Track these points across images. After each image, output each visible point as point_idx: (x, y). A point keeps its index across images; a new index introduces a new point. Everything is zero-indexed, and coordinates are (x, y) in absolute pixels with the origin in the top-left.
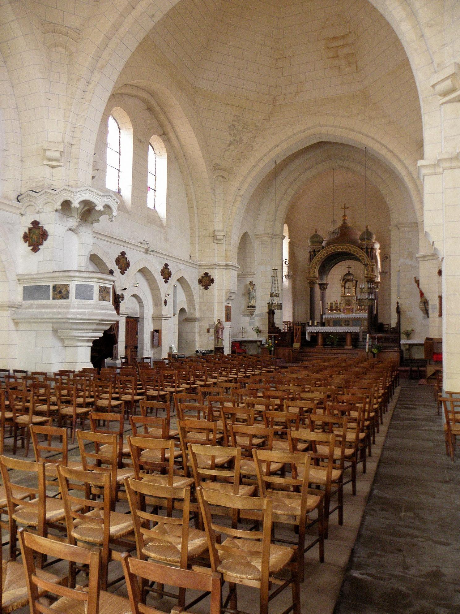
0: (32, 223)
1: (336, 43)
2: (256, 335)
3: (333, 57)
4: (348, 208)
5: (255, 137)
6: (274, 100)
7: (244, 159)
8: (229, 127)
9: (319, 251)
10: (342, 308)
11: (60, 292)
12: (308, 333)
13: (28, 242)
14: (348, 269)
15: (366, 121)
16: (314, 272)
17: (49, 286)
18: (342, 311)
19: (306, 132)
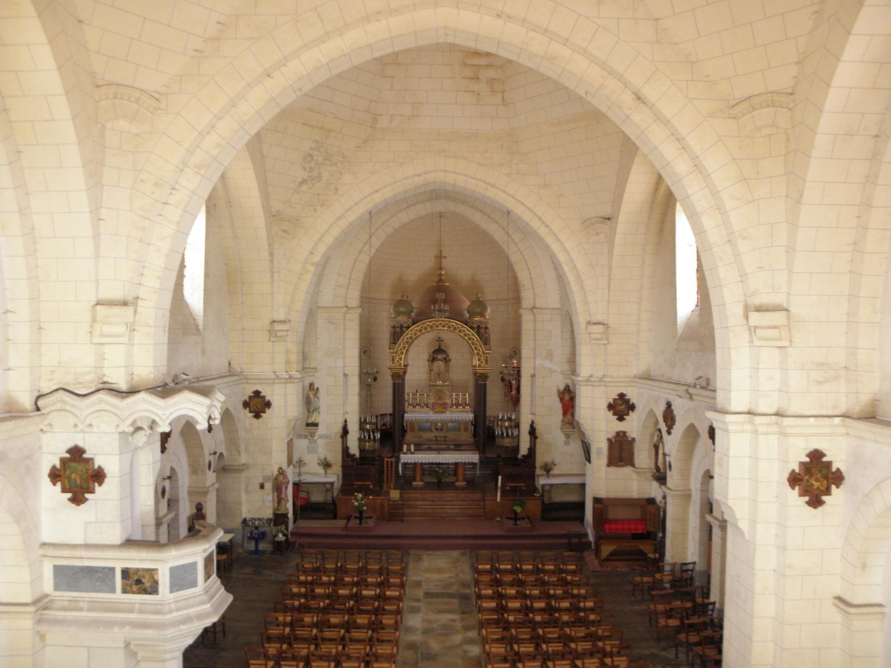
1: (477, 61)
2: (321, 470)
3: (472, 78)
5: (341, 173)
6: (375, 120)
7: (323, 205)
8: (304, 158)
9: (408, 327)
10: (431, 401)
11: (139, 582)
12: (402, 464)
13: (59, 484)
14: (438, 342)
16: (401, 359)
17: (112, 570)
18: (430, 406)
19: (422, 177)
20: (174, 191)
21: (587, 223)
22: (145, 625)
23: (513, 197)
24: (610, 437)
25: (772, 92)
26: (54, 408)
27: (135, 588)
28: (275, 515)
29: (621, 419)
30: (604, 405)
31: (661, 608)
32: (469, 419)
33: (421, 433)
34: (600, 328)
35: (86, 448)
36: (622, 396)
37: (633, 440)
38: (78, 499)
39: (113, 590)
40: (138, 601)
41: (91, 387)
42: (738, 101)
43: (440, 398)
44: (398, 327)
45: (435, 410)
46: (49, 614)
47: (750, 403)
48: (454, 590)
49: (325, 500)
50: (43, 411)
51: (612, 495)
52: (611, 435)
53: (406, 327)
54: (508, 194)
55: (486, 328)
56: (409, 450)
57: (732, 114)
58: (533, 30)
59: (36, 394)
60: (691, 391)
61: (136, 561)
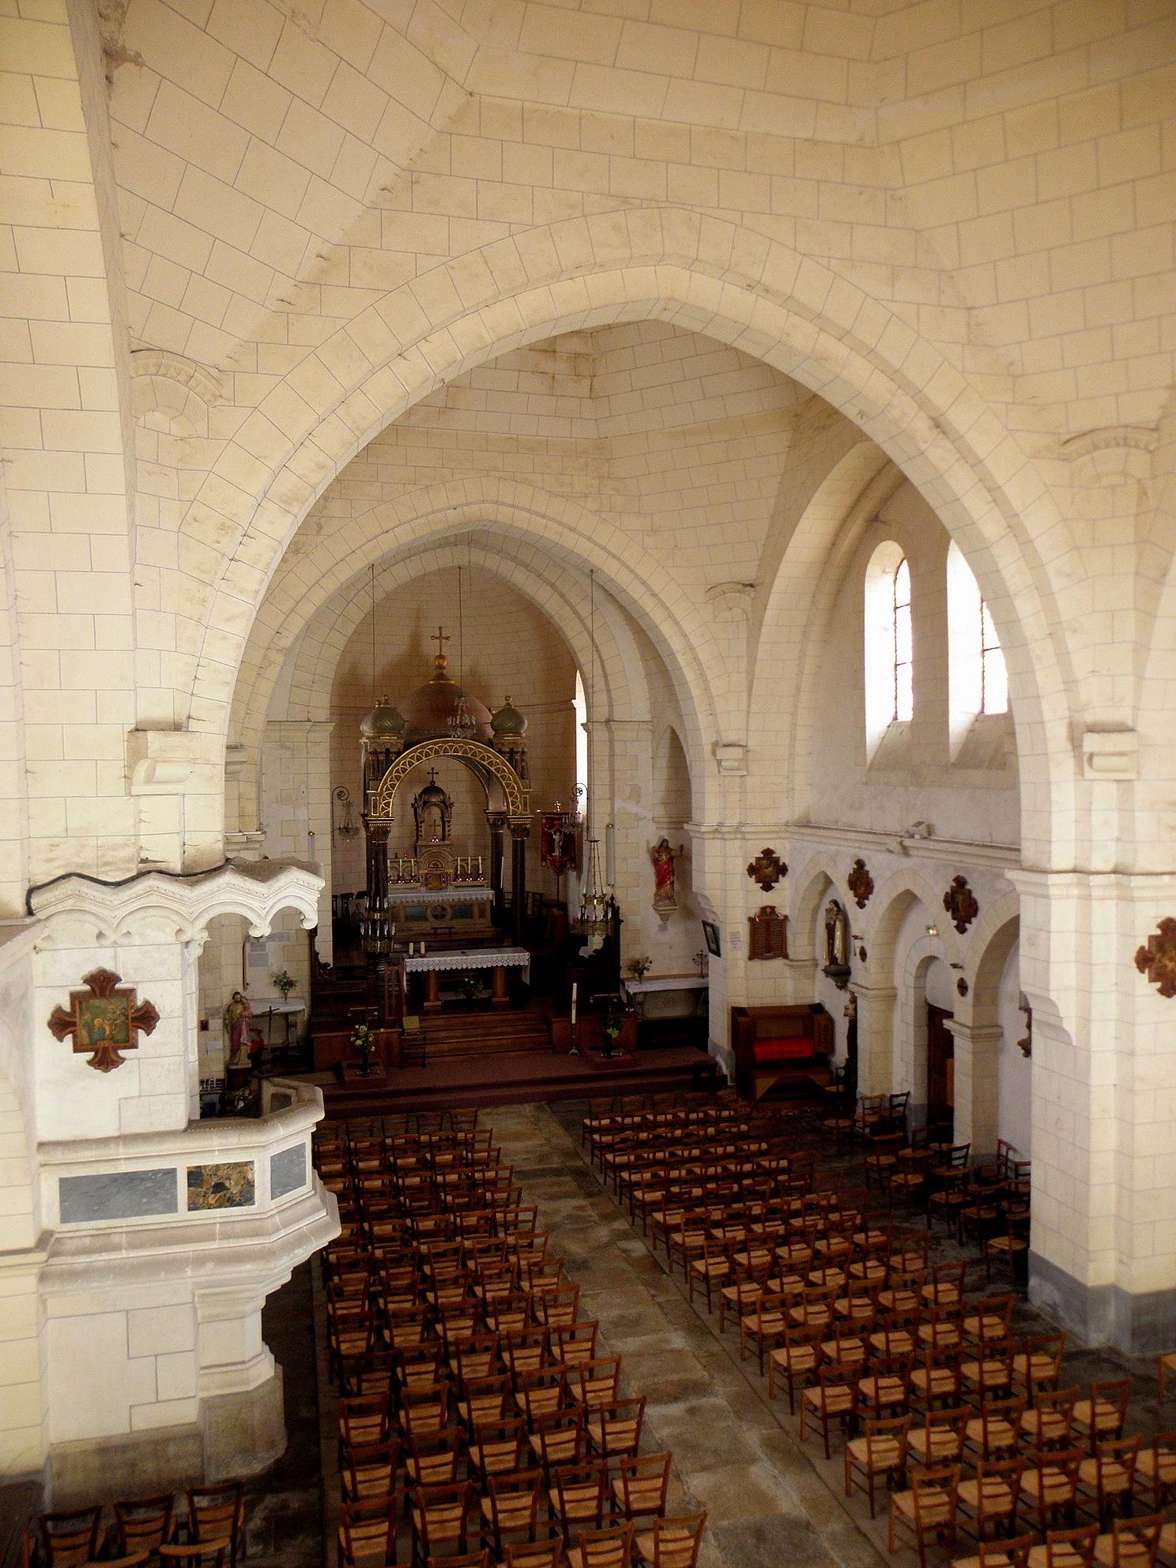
0: (90, 980)
2: (274, 993)
4: (447, 638)
9: (399, 754)
11: (219, 1187)
13: (69, 1038)
15: (603, 515)
16: (387, 805)
17: (172, 1172)
19: (459, 510)
20: (246, 540)
21: (715, 590)
22: (239, 1258)
23: (603, 548)
24: (752, 916)
25: (1126, 426)
26: (60, 907)
27: (212, 1199)
28: (228, 1070)
29: (767, 887)
30: (741, 867)
31: (885, 1160)
32: (488, 898)
33: (411, 924)
34: (736, 753)
35: (120, 973)
36: (768, 853)
37: (786, 917)
38: (105, 1060)
39: (172, 1207)
40: (218, 1220)
41: (128, 870)
42: (1073, 435)
43: (436, 866)
44: (381, 753)
45: (430, 886)
46: (62, 1262)
47: (1076, 857)
48: (556, 1162)
49: (283, 1043)
50: (40, 915)
51: (756, 1002)
52: (753, 912)
53: (395, 753)
54: (596, 543)
55: (523, 753)
56: (417, 951)
57: (1064, 454)
58: (796, 314)
59: (27, 887)
60: (907, 842)
61: (122, 1162)
